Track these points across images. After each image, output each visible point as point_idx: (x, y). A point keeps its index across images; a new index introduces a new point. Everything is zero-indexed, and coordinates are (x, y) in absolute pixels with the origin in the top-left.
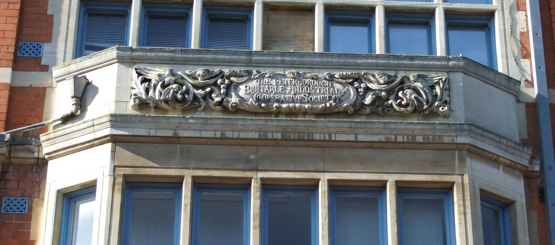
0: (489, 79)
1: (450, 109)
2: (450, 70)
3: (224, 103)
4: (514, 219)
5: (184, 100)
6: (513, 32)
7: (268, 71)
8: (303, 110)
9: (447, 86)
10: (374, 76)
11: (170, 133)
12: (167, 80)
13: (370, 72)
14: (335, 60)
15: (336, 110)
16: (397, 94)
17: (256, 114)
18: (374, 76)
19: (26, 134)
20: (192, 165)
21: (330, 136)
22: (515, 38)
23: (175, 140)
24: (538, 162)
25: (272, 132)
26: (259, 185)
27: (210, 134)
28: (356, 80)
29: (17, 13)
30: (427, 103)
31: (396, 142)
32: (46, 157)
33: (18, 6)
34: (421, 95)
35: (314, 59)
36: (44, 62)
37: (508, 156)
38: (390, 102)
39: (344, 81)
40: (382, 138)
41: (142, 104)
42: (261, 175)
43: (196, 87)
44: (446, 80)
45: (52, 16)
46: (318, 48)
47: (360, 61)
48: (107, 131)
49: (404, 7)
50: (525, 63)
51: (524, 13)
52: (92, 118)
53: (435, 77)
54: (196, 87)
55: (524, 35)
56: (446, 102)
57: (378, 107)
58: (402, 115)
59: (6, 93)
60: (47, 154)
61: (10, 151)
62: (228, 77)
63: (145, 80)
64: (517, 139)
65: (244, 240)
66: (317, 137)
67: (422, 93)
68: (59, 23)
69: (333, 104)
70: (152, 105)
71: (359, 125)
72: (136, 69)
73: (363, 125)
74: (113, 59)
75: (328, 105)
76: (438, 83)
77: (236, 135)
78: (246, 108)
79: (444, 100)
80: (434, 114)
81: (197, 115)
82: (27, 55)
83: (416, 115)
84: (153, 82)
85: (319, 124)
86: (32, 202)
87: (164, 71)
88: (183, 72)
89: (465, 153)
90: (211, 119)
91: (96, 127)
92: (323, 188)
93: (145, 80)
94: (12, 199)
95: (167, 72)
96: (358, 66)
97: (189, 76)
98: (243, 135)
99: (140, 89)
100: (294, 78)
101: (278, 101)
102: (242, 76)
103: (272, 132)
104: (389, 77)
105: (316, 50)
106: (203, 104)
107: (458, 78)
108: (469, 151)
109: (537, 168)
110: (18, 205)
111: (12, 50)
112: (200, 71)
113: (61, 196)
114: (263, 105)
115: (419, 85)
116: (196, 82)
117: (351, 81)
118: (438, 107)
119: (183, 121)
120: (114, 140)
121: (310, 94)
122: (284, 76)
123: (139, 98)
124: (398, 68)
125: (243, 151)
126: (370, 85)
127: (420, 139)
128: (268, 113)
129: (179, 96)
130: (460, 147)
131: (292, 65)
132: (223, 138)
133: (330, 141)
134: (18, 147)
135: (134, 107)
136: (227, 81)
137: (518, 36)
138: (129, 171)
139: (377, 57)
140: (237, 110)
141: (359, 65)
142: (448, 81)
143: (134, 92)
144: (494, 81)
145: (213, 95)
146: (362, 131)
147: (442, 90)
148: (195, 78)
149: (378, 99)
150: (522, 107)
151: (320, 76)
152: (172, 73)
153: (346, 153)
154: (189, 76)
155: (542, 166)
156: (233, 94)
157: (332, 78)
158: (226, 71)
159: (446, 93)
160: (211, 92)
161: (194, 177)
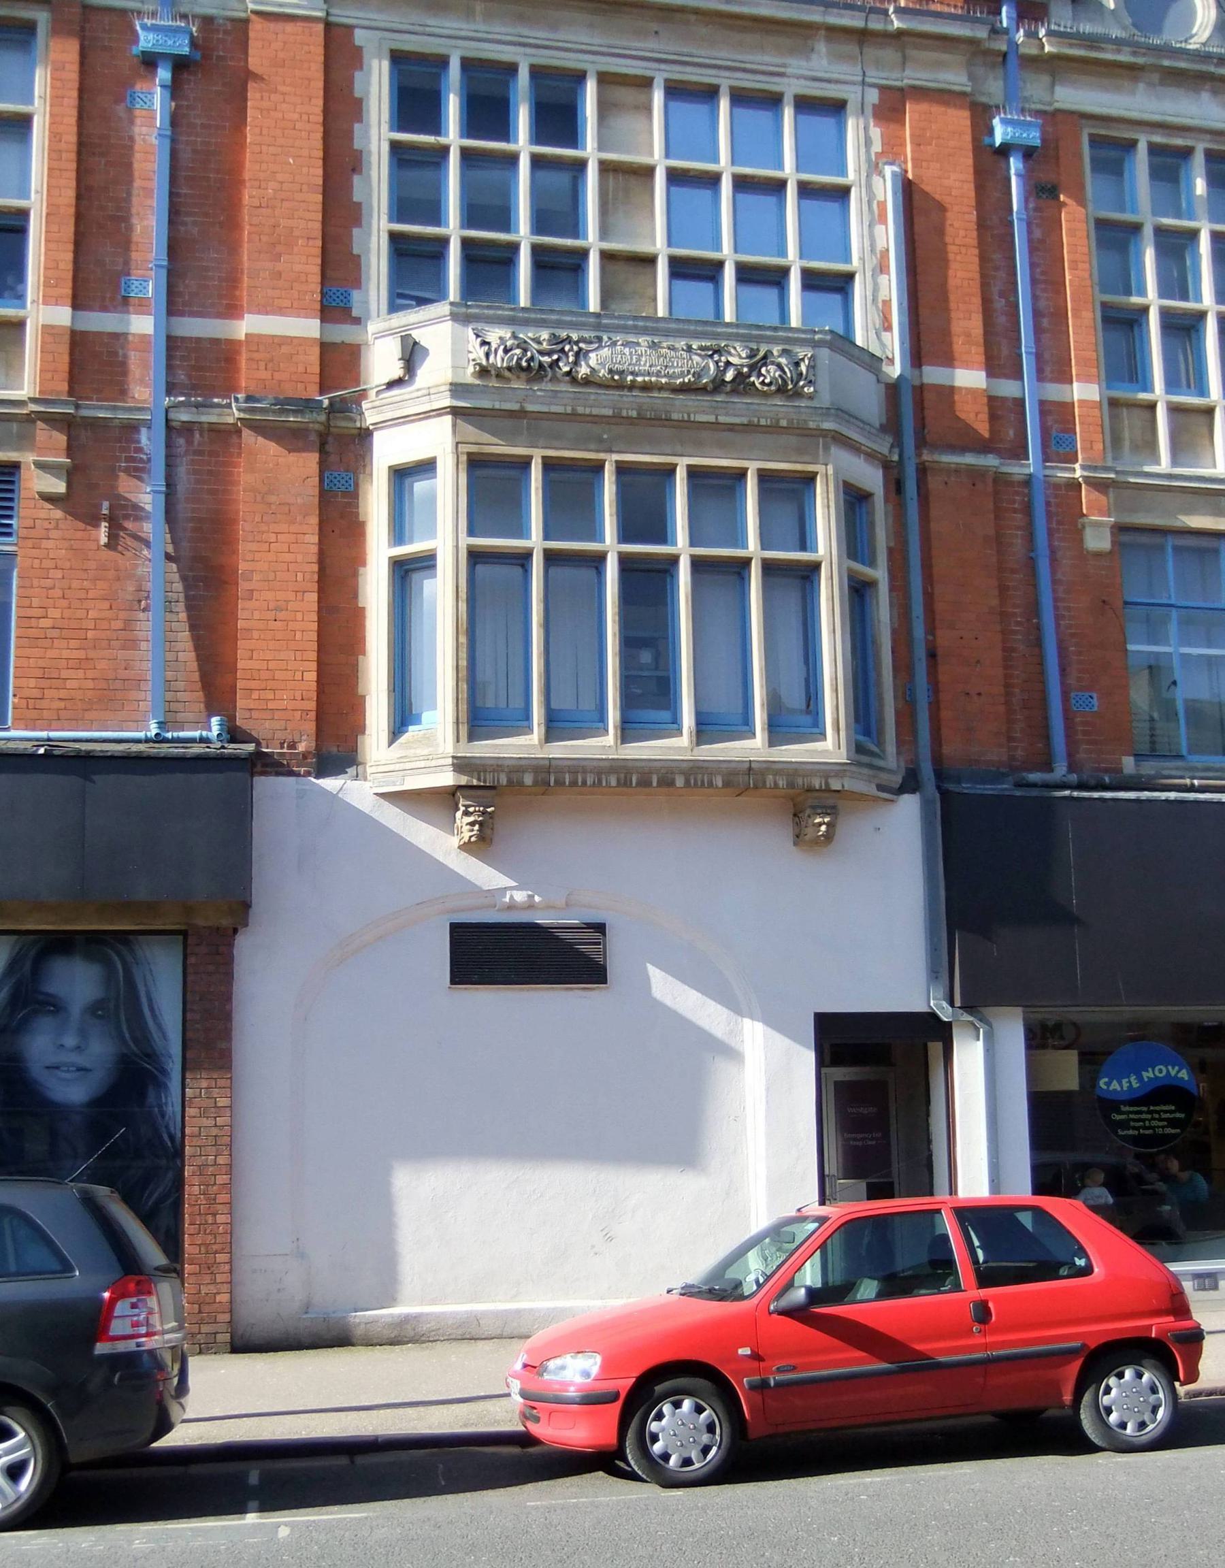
0: (853, 356)
1: (815, 391)
2: (815, 344)
3: (574, 374)
4: (871, 513)
5: (529, 368)
6: (874, 300)
7: (617, 337)
8: (659, 385)
9: (812, 364)
10: (735, 348)
11: (516, 407)
12: (509, 343)
13: (730, 343)
14: (692, 328)
15: (695, 386)
16: (760, 371)
17: (607, 387)
18: (735, 348)
19: (343, 399)
20: (541, 443)
21: (689, 416)
22: (877, 307)
23: (521, 414)
24: (896, 450)
25: (627, 409)
26: (614, 468)
27: (560, 409)
28: (715, 352)
29: (318, 251)
30: (792, 381)
31: (759, 426)
32: (371, 427)
33: (319, 243)
34: (785, 373)
35: (670, 326)
36: (355, 313)
37: (869, 444)
38: (752, 379)
39: (703, 353)
40: (745, 420)
41: (483, 372)
42: (616, 457)
43: (541, 353)
44: (812, 356)
45: (359, 256)
46: (661, 312)
47: (719, 330)
48: (447, 402)
49: (756, 263)
50: (886, 336)
51: (887, 277)
52: (427, 386)
53: (803, 352)
54: (541, 353)
55: (887, 303)
56: (810, 382)
57: (739, 385)
58: (765, 395)
59: (316, 351)
60: (372, 424)
61: (328, 419)
62: (577, 343)
63: (484, 343)
64: (877, 425)
65: (598, 528)
66: (675, 416)
67: (787, 370)
68: (369, 266)
69: (692, 379)
70: (493, 372)
71: (720, 404)
72: (473, 329)
73: (724, 405)
74: (445, 316)
75: (686, 380)
76: (803, 360)
77: (588, 411)
78: (597, 380)
79: (809, 379)
80: (798, 394)
81: (543, 386)
82: (334, 304)
83: (779, 396)
84: (494, 346)
85: (677, 403)
86: (358, 479)
87: (505, 332)
88: (527, 334)
89: (829, 439)
90: (561, 392)
91: (432, 396)
92: (681, 476)
93: (484, 343)
94: (336, 474)
95: (509, 335)
96: (716, 336)
97: (533, 340)
98: (595, 411)
99: (479, 353)
100: (649, 347)
101: (632, 373)
102: (591, 343)
103: (627, 409)
104: (752, 350)
105: (660, 314)
106: (550, 375)
107: (824, 353)
108: (833, 438)
109: (895, 458)
110: (343, 482)
111: (318, 297)
112: (545, 335)
113: (392, 473)
114: (616, 377)
115: (783, 361)
116: (541, 348)
117: (710, 353)
118: (803, 387)
119: (530, 393)
120: (455, 412)
121: (666, 367)
122: (638, 344)
123: (480, 365)
124: (760, 339)
125: (596, 429)
126: (731, 359)
127: (784, 423)
128: (620, 386)
129: (524, 364)
130: (824, 433)
131: (645, 331)
132: (574, 414)
133: (689, 421)
134: (338, 415)
135: (473, 374)
136: (575, 348)
137: (880, 305)
138: (473, 449)
139: (728, 325)
140: (587, 382)
141: (719, 334)
142: (812, 358)
143: (471, 356)
144: (858, 359)
145: (561, 364)
146: (724, 411)
147: (808, 367)
148: (539, 343)
149: (739, 376)
150: (883, 385)
151: (677, 345)
152: (514, 336)
153: (705, 434)
154: (533, 340)
155: (901, 456)
156: (583, 363)
157: (689, 349)
158: (575, 336)
159: (811, 371)
160: (558, 360)
161: (544, 458)
